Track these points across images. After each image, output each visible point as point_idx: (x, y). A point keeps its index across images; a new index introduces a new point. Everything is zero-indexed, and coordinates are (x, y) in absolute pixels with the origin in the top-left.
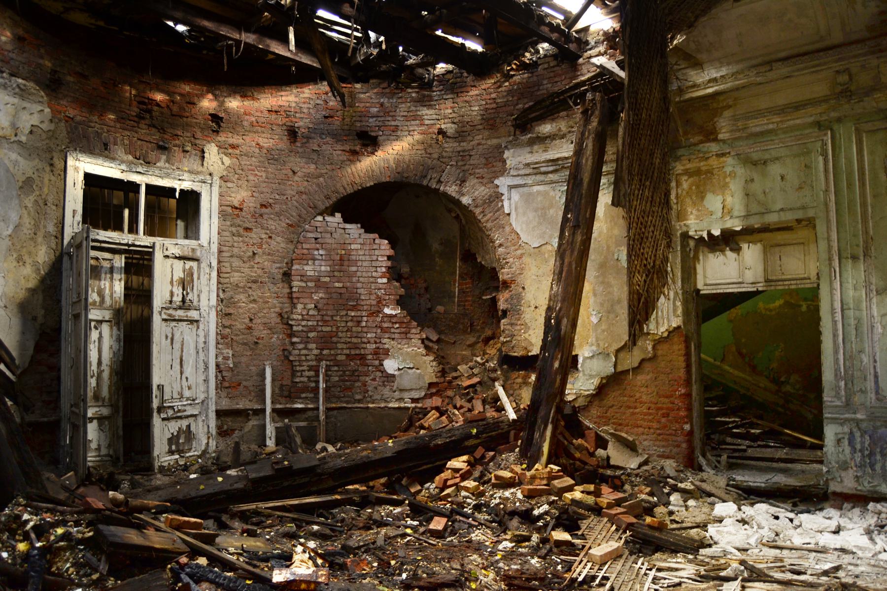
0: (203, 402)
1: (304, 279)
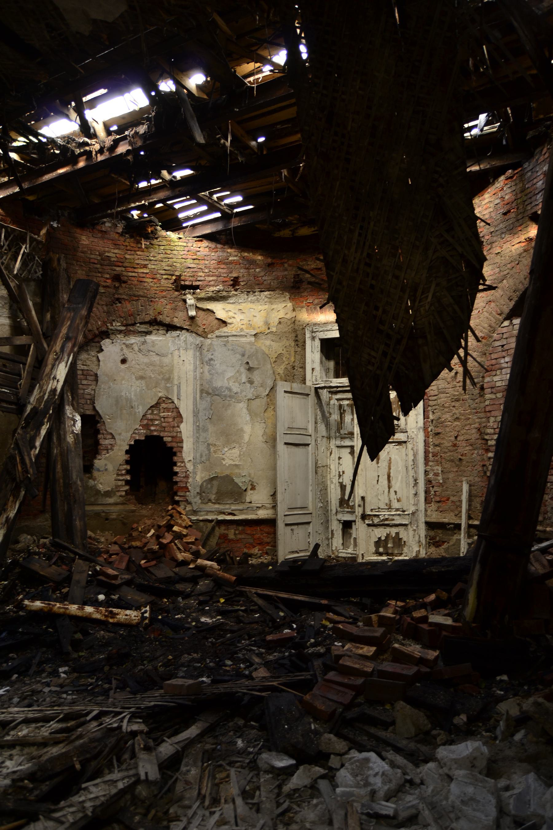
0: (413, 514)
1: (494, 390)
